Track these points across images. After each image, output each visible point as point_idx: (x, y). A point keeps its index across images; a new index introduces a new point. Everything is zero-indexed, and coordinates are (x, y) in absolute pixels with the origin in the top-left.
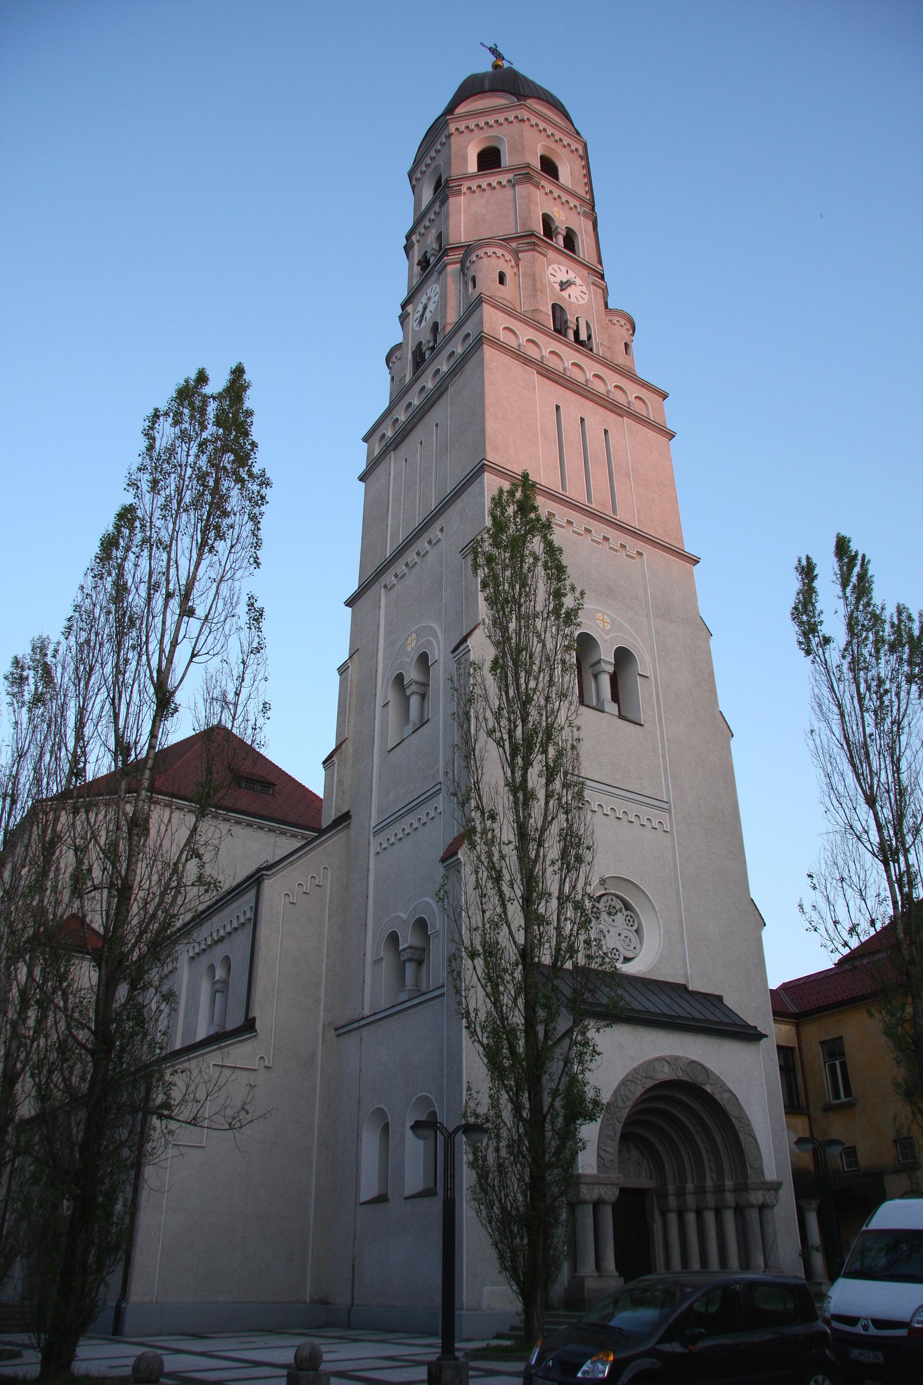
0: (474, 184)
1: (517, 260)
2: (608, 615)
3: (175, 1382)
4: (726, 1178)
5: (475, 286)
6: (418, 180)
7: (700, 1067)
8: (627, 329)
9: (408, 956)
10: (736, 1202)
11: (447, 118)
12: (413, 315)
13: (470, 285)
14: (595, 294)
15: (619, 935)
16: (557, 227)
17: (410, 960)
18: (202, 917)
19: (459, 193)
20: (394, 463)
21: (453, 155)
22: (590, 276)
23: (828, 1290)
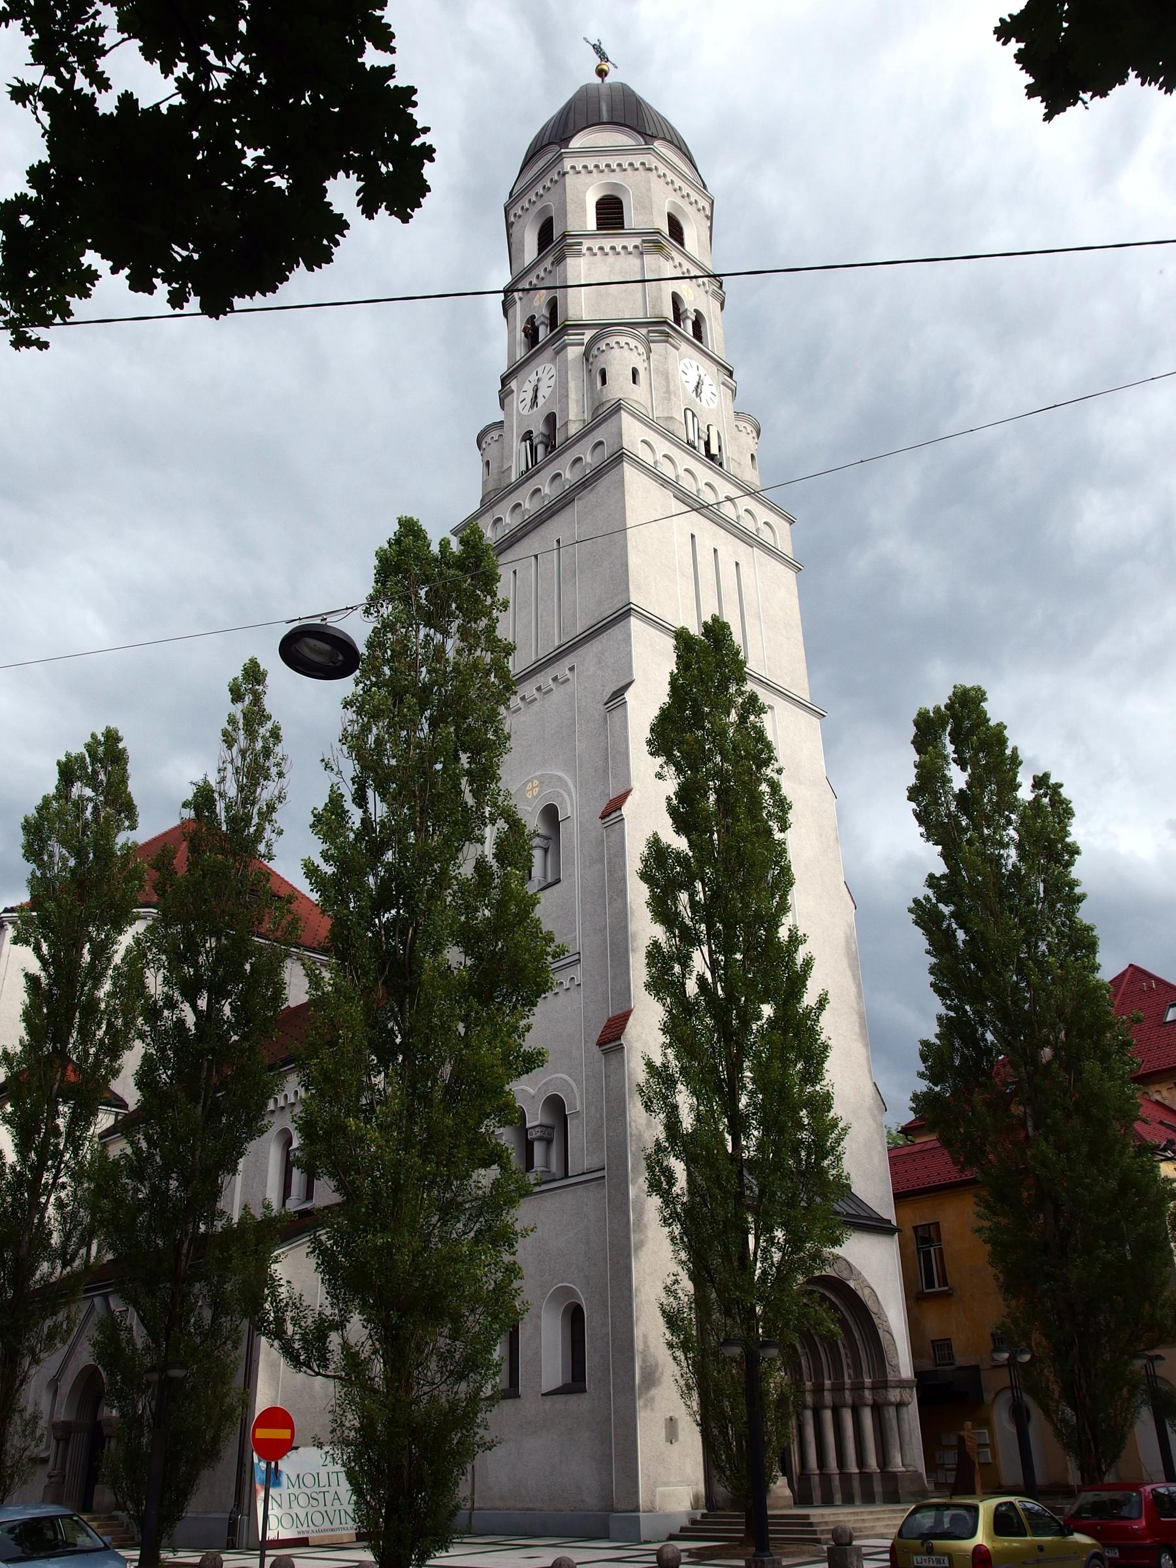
0: (595, 244)
1: (649, 351)
4: (864, 1376)
9: (539, 1134)
10: (874, 1400)
11: (563, 151)
14: (725, 395)
17: (540, 1139)
19: (579, 254)
21: (568, 200)
22: (720, 373)
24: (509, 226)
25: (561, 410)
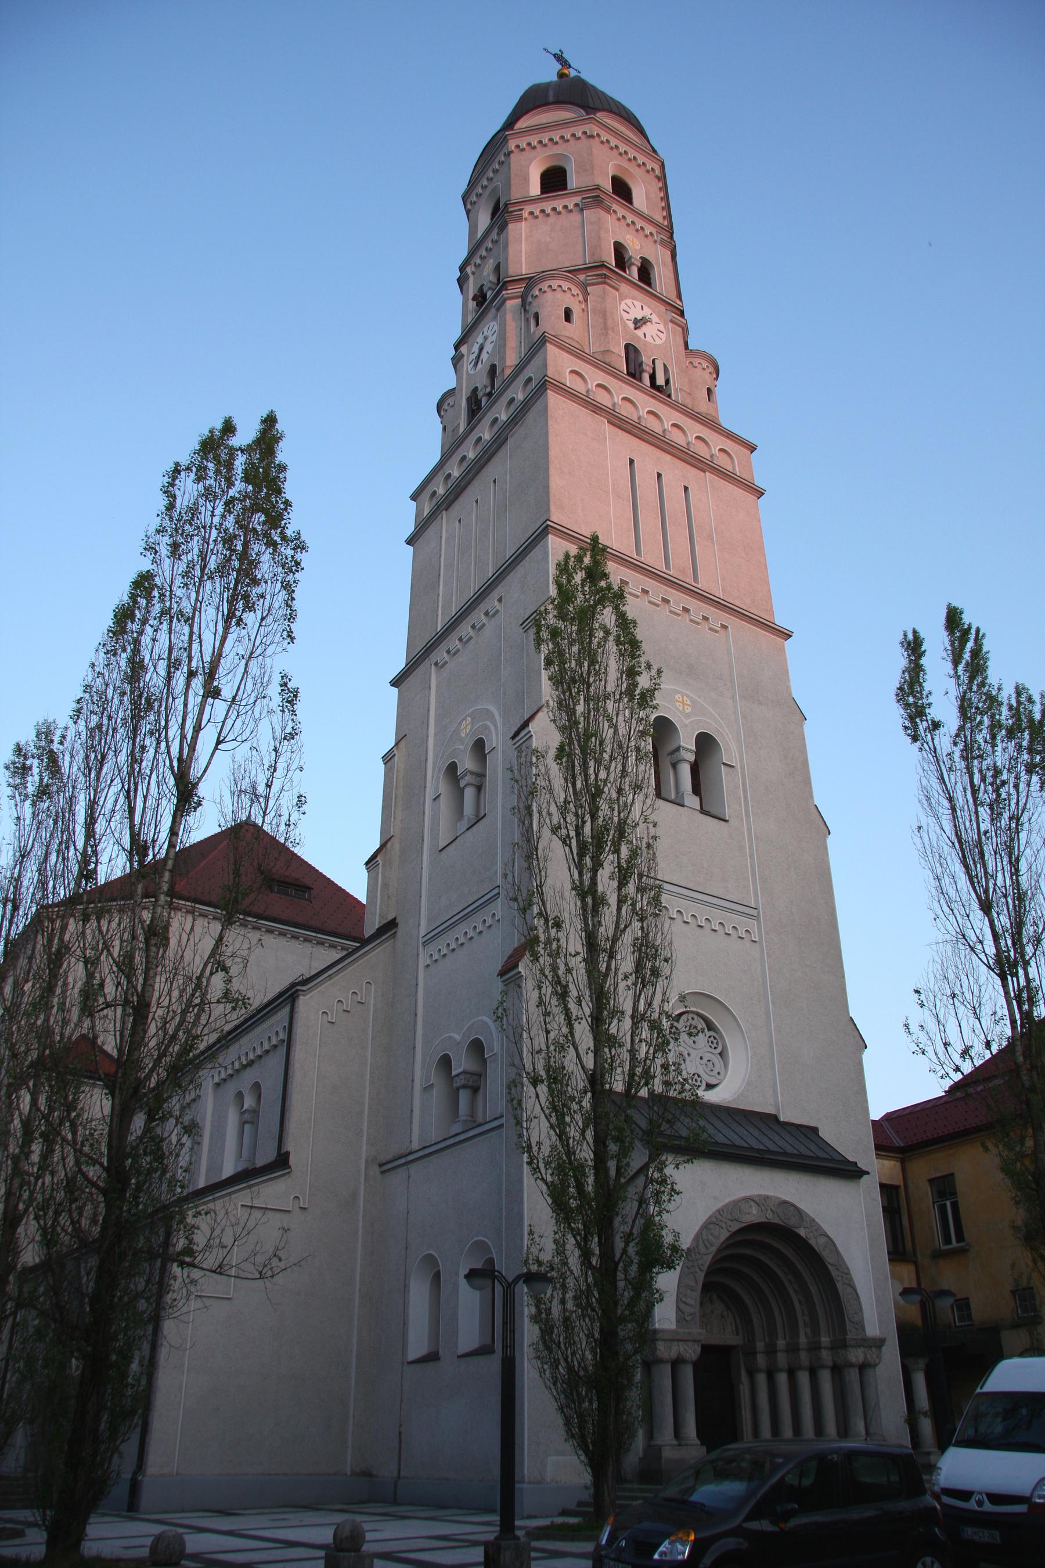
0: (536, 209)
1: (586, 294)
2: (688, 696)
3: (199, 1565)
4: (822, 1333)
5: (537, 324)
6: (473, 203)
7: (792, 1208)
8: (710, 373)
9: (462, 1082)
10: (833, 1361)
12: (468, 357)
13: (533, 322)
14: (674, 333)
15: (701, 1058)
16: (631, 257)
18: (229, 1038)
19: (520, 218)
20: (446, 524)
21: (513, 175)
22: (668, 312)
23: (937, 1461)
24: (468, 212)
25: (500, 360)
